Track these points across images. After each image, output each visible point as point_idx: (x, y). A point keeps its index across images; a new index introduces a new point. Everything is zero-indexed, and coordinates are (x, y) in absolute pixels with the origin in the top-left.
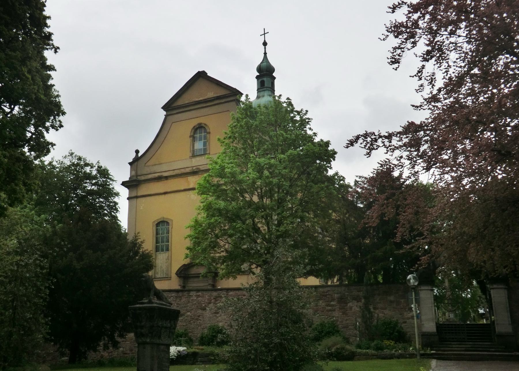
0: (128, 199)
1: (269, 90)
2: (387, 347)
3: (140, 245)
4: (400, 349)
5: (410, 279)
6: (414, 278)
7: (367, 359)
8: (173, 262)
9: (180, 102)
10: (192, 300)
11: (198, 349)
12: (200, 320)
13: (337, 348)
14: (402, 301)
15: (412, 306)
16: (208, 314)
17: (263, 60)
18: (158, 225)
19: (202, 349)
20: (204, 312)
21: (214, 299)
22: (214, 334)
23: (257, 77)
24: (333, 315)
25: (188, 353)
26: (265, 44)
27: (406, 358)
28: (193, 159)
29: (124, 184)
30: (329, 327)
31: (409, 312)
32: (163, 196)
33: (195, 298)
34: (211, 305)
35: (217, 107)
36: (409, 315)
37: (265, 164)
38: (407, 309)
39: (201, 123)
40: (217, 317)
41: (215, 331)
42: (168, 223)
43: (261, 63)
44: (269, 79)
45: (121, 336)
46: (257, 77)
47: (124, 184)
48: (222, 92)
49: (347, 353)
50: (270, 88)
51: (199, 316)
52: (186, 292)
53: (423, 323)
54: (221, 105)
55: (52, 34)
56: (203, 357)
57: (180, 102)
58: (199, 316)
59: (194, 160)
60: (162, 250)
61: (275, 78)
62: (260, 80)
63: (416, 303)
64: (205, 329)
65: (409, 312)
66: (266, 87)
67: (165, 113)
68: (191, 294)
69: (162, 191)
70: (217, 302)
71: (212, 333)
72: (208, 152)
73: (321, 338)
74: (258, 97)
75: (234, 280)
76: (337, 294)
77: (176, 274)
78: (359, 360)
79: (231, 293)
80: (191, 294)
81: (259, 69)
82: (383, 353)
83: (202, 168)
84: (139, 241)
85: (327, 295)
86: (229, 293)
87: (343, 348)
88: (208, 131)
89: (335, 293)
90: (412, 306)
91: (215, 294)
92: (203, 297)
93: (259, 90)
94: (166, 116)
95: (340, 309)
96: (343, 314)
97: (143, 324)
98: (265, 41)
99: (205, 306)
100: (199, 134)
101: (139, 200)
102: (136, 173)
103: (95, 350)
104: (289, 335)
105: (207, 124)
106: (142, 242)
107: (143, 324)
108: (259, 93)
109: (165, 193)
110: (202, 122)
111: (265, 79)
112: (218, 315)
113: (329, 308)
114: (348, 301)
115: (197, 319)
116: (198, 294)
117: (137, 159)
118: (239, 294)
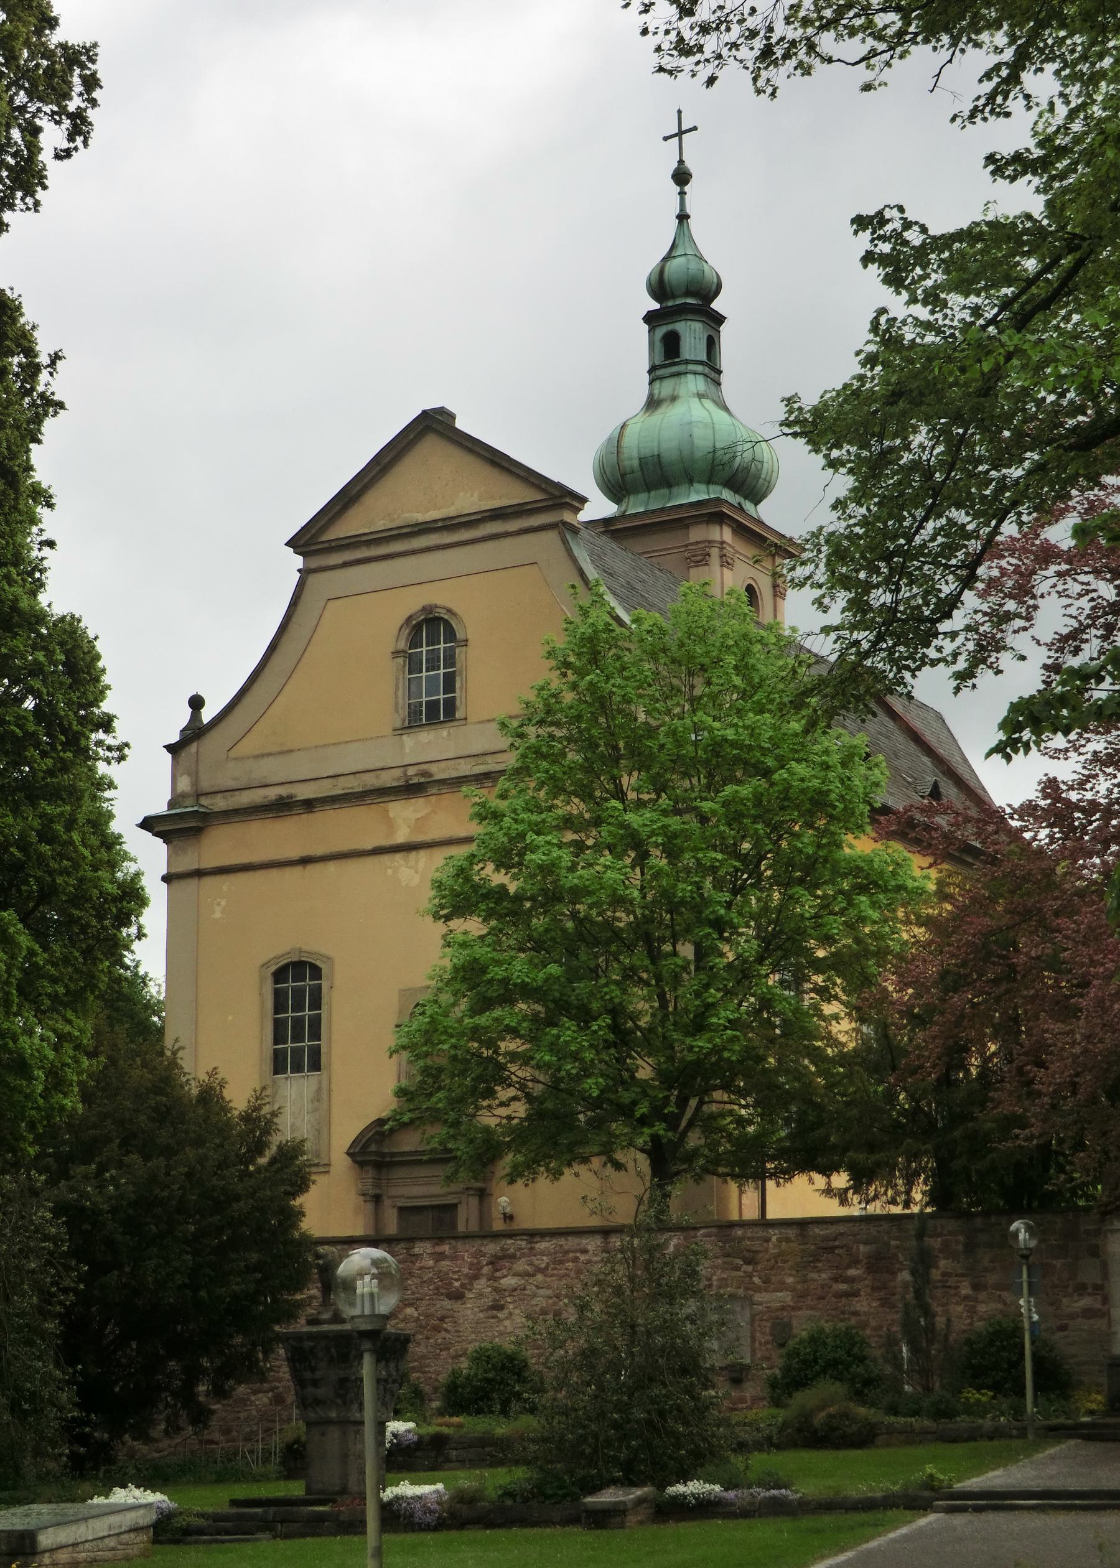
0: (166, 879)
1: (695, 373)
2: (969, 1410)
3: (269, 1122)
4: (1003, 1414)
5: (1018, 1231)
6: (1029, 1229)
7: (909, 1442)
8: (335, 1110)
9: (352, 525)
10: (421, 1268)
11: (447, 1426)
12: (446, 1330)
13: (830, 1416)
14: (1058, 1263)
15: (1022, 1302)
16: (469, 1312)
17: (674, 246)
18: (280, 975)
19: (460, 1426)
20: (457, 1305)
21: (491, 1263)
22: (490, 1375)
23: (651, 318)
24: (852, 1309)
25: (421, 1437)
26: (681, 177)
27: (1011, 1437)
28: (405, 737)
29: (148, 824)
30: (837, 1347)
31: (1076, 1298)
32: (298, 870)
33: (431, 1263)
34: (481, 1284)
35: (490, 545)
36: (1075, 1305)
37: (653, 833)
38: (1070, 1290)
39: (436, 606)
40: (500, 1321)
41: (493, 1366)
42: (316, 972)
43: (665, 259)
44: (697, 326)
45: (220, 1392)
46: (651, 318)
47: (148, 824)
48: (515, 494)
49: (855, 1428)
50: (701, 363)
51: (442, 1319)
52: (403, 1245)
53: (1113, 1330)
54: (506, 543)
55: (115, 716)
56: (464, 1448)
57: (352, 525)
58: (442, 1319)
59: (408, 741)
60: (297, 1068)
61: (719, 319)
62: (661, 332)
63: (1030, 1294)
64: (462, 1359)
65: (1076, 1298)
66: (687, 362)
67: (299, 561)
68: (416, 1250)
69: (295, 854)
70: (498, 1274)
71: (486, 1371)
72: (458, 715)
73: (811, 1379)
74: (653, 404)
75: (552, 1181)
76: (866, 1243)
77: (348, 1153)
78: (888, 1445)
79: (542, 1245)
80: (416, 1250)
81: (659, 287)
82: (950, 1426)
83: (439, 772)
84: (266, 1110)
85: (836, 1247)
86: (537, 1246)
87: (845, 1415)
88: (460, 635)
89: (859, 1242)
90: (1022, 1302)
91: (492, 1248)
92: (454, 1258)
93: (655, 372)
94: (305, 573)
95: (874, 1289)
96: (882, 1306)
97: (319, 1374)
98: (681, 162)
99: (463, 1286)
100: (427, 645)
101: (208, 881)
102: (195, 783)
103: (142, 1435)
104: (666, 1403)
105: (455, 609)
106: (274, 1114)
107: (319, 1374)
108: (657, 384)
109: (305, 861)
110: (439, 602)
111: (680, 327)
112: (501, 1315)
113: (843, 1287)
114: (897, 1266)
115: (437, 1329)
116: (439, 1249)
117: (194, 732)
118: (566, 1247)
